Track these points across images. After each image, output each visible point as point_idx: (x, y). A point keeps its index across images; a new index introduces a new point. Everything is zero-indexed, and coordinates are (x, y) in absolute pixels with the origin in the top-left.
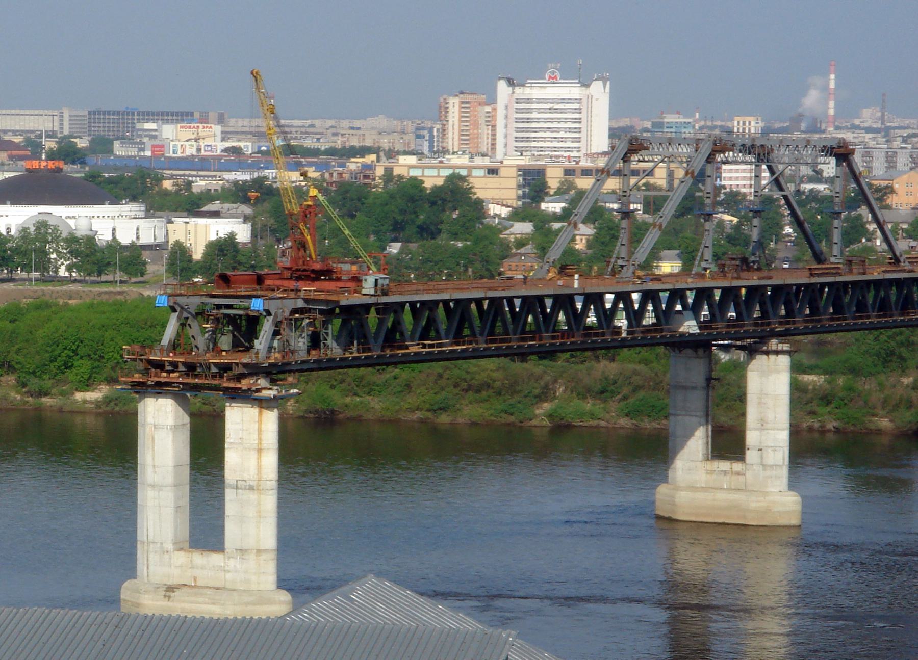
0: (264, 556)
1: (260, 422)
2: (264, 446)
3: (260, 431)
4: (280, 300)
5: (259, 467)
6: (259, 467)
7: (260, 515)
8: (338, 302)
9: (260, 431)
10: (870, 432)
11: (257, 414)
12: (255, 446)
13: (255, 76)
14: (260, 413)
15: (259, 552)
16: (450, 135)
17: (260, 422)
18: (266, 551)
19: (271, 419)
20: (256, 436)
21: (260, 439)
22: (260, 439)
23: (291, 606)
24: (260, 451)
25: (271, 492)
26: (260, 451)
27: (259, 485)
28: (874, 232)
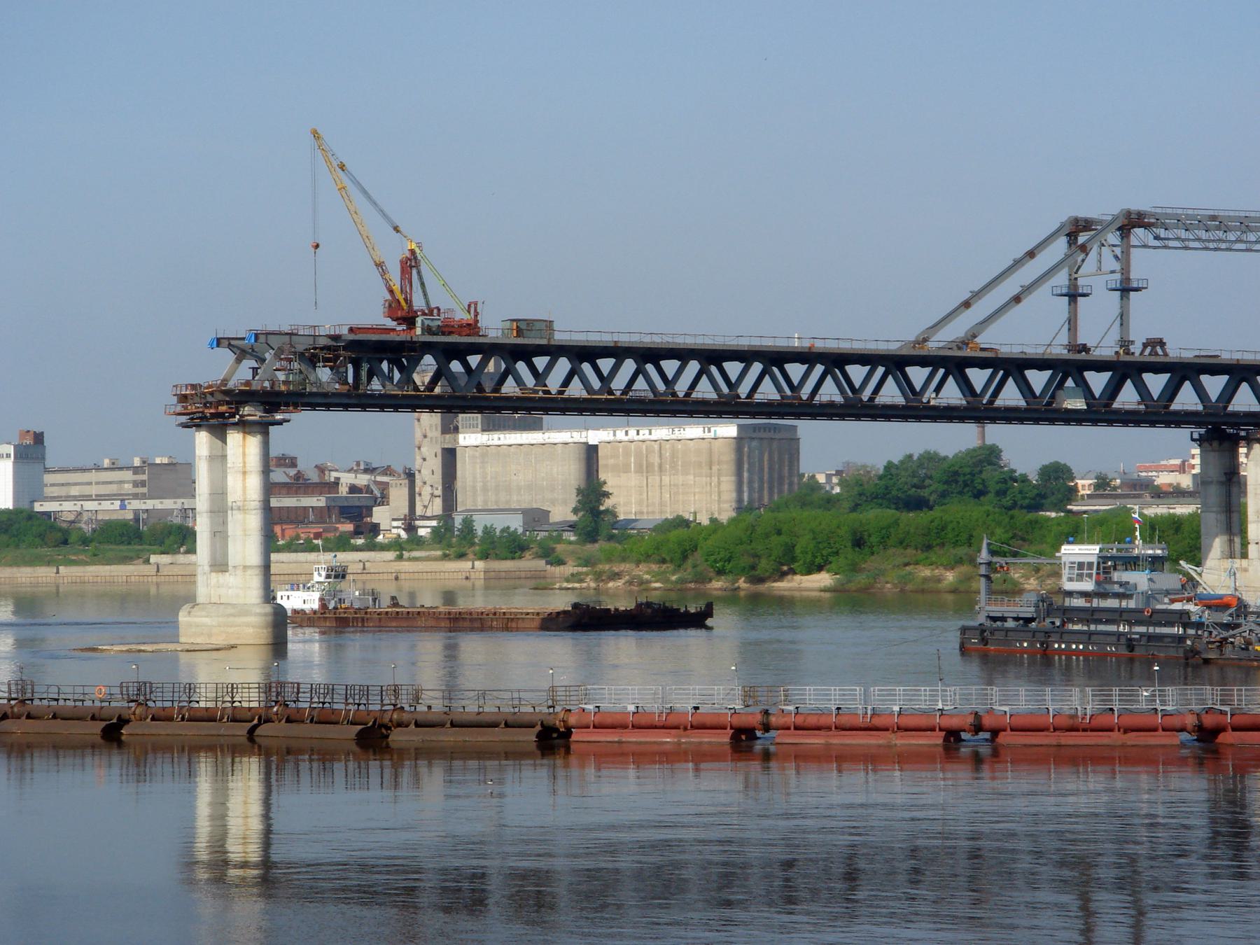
0: (249, 572)
1: (244, 446)
2: (248, 469)
3: (244, 454)
4: (238, 336)
5: (244, 488)
6: (244, 488)
7: (245, 534)
8: (134, 474)
9: (244, 454)
10: (831, 744)
11: (241, 438)
12: (241, 469)
13: (315, 134)
14: (244, 438)
15: (245, 568)
16: (669, 837)
17: (244, 446)
18: (249, 567)
19: (151, 556)
20: (241, 460)
21: (244, 463)
22: (244, 463)
23: (270, 630)
24: (244, 473)
25: (254, 512)
26: (244, 473)
27: (244, 506)
28: (1091, 602)
